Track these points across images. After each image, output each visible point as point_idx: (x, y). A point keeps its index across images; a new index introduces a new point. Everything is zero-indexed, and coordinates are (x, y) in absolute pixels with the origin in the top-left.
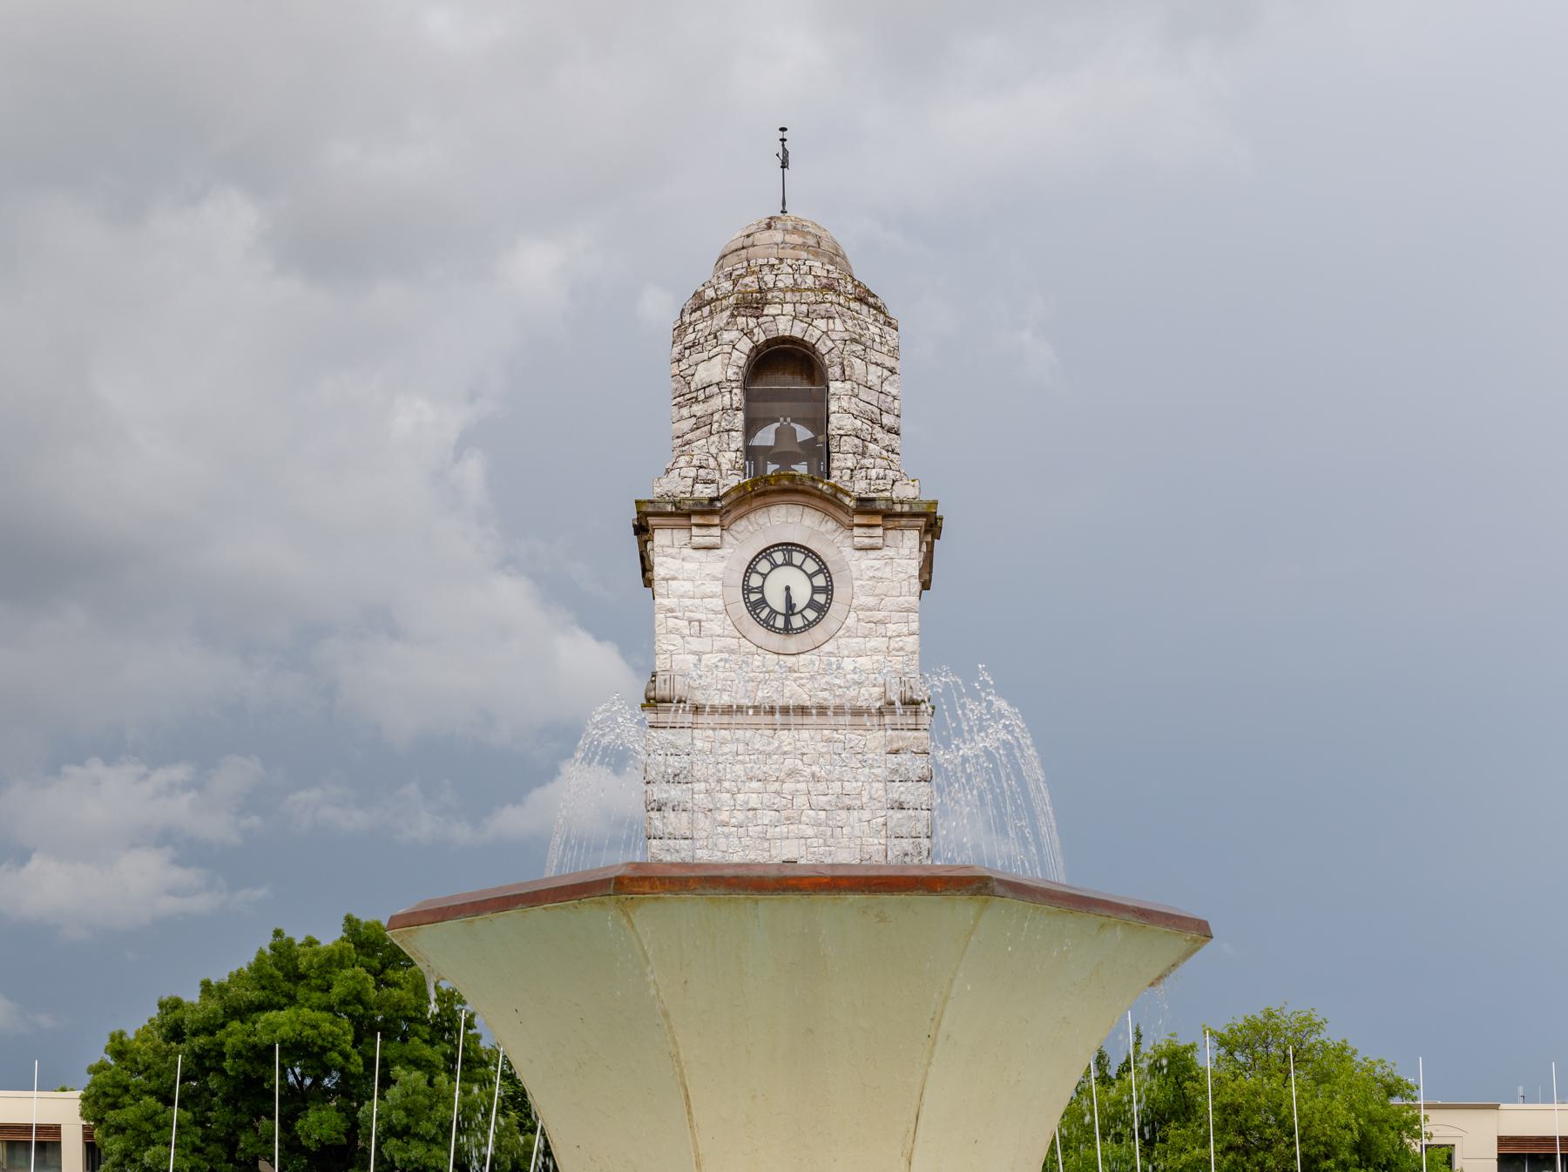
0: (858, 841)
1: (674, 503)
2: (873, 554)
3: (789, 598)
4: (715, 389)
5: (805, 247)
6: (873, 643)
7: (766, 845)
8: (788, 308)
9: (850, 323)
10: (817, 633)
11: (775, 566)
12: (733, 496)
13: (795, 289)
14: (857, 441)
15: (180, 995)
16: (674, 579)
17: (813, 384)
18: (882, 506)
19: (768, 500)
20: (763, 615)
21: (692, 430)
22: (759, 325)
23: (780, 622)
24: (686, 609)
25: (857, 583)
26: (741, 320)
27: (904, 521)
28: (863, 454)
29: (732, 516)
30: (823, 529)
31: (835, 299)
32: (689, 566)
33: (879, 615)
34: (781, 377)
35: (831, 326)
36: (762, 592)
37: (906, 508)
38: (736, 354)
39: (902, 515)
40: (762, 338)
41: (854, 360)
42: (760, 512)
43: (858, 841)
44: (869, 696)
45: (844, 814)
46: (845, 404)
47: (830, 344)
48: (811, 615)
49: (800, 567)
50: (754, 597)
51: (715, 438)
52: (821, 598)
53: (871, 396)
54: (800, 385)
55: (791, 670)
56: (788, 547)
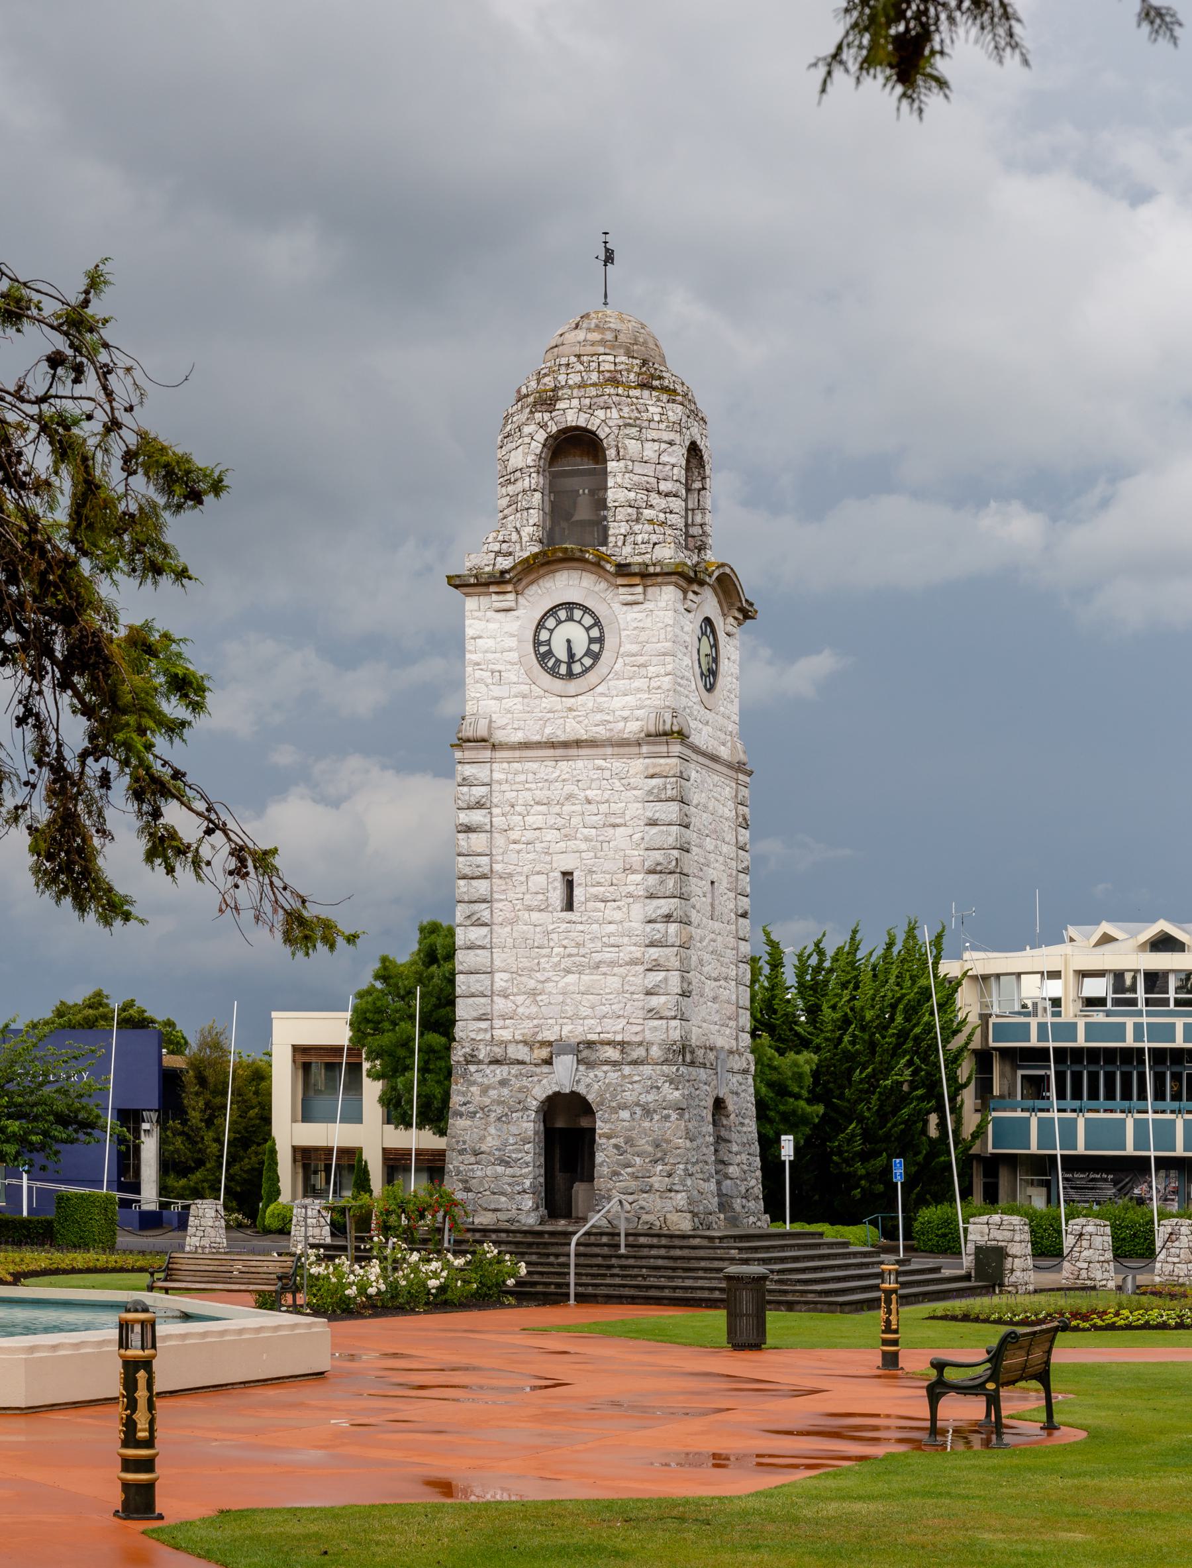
0: (622, 853)
1: (476, 576)
2: (636, 608)
3: (570, 649)
4: (518, 474)
5: (603, 342)
6: (637, 683)
7: (548, 858)
8: (575, 402)
9: (626, 409)
10: (592, 677)
11: (559, 622)
12: (519, 568)
13: (582, 385)
14: (630, 510)
15: (439, 920)
16: (480, 637)
17: (597, 463)
18: (636, 569)
19: (553, 567)
20: (550, 664)
21: (509, 506)
22: (552, 419)
23: (563, 669)
24: (489, 662)
25: (624, 633)
26: (538, 415)
27: (659, 579)
28: (637, 520)
29: (524, 582)
30: (596, 589)
31: (612, 391)
32: (492, 626)
33: (641, 660)
34: (571, 459)
35: (609, 415)
36: (549, 645)
37: (658, 569)
38: (534, 443)
39: (656, 575)
40: (555, 429)
41: (627, 441)
42: (547, 578)
43: (622, 853)
44: (633, 728)
45: (611, 831)
46: (619, 480)
47: (607, 430)
48: (588, 662)
49: (579, 622)
50: (543, 649)
51: (518, 515)
52: (595, 647)
53: (649, 469)
54: (587, 465)
55: (570, 709)
56: (570, 606)
